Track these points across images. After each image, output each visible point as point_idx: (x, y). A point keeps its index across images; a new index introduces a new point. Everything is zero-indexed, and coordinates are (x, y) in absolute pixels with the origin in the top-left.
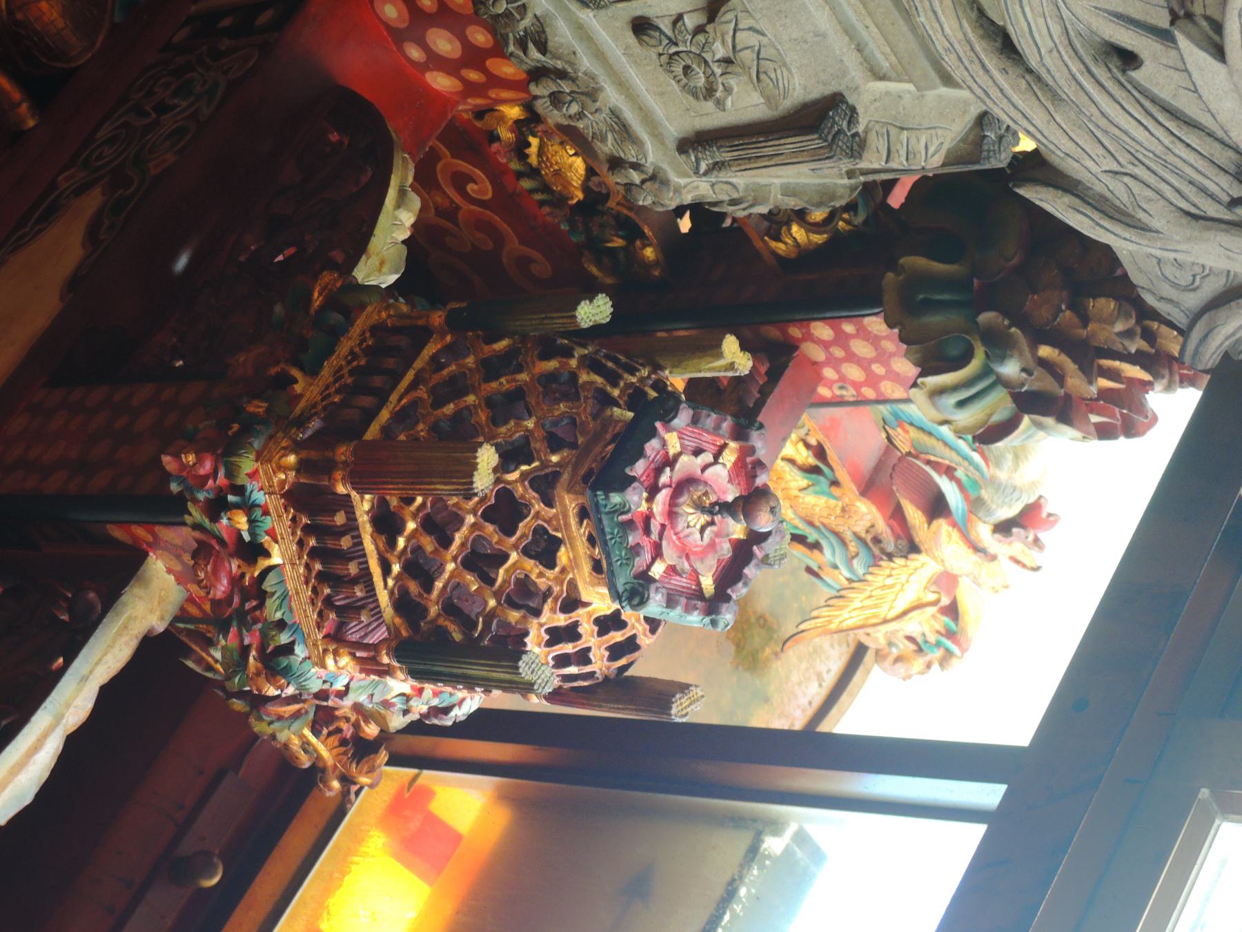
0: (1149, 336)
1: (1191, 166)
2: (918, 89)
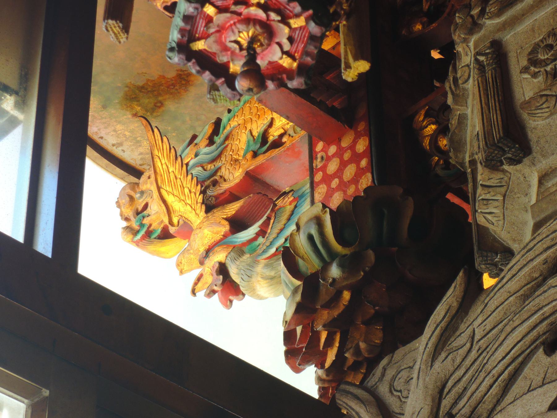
0: (356, 366)
1: (477, 389)
2: (532, 207)
